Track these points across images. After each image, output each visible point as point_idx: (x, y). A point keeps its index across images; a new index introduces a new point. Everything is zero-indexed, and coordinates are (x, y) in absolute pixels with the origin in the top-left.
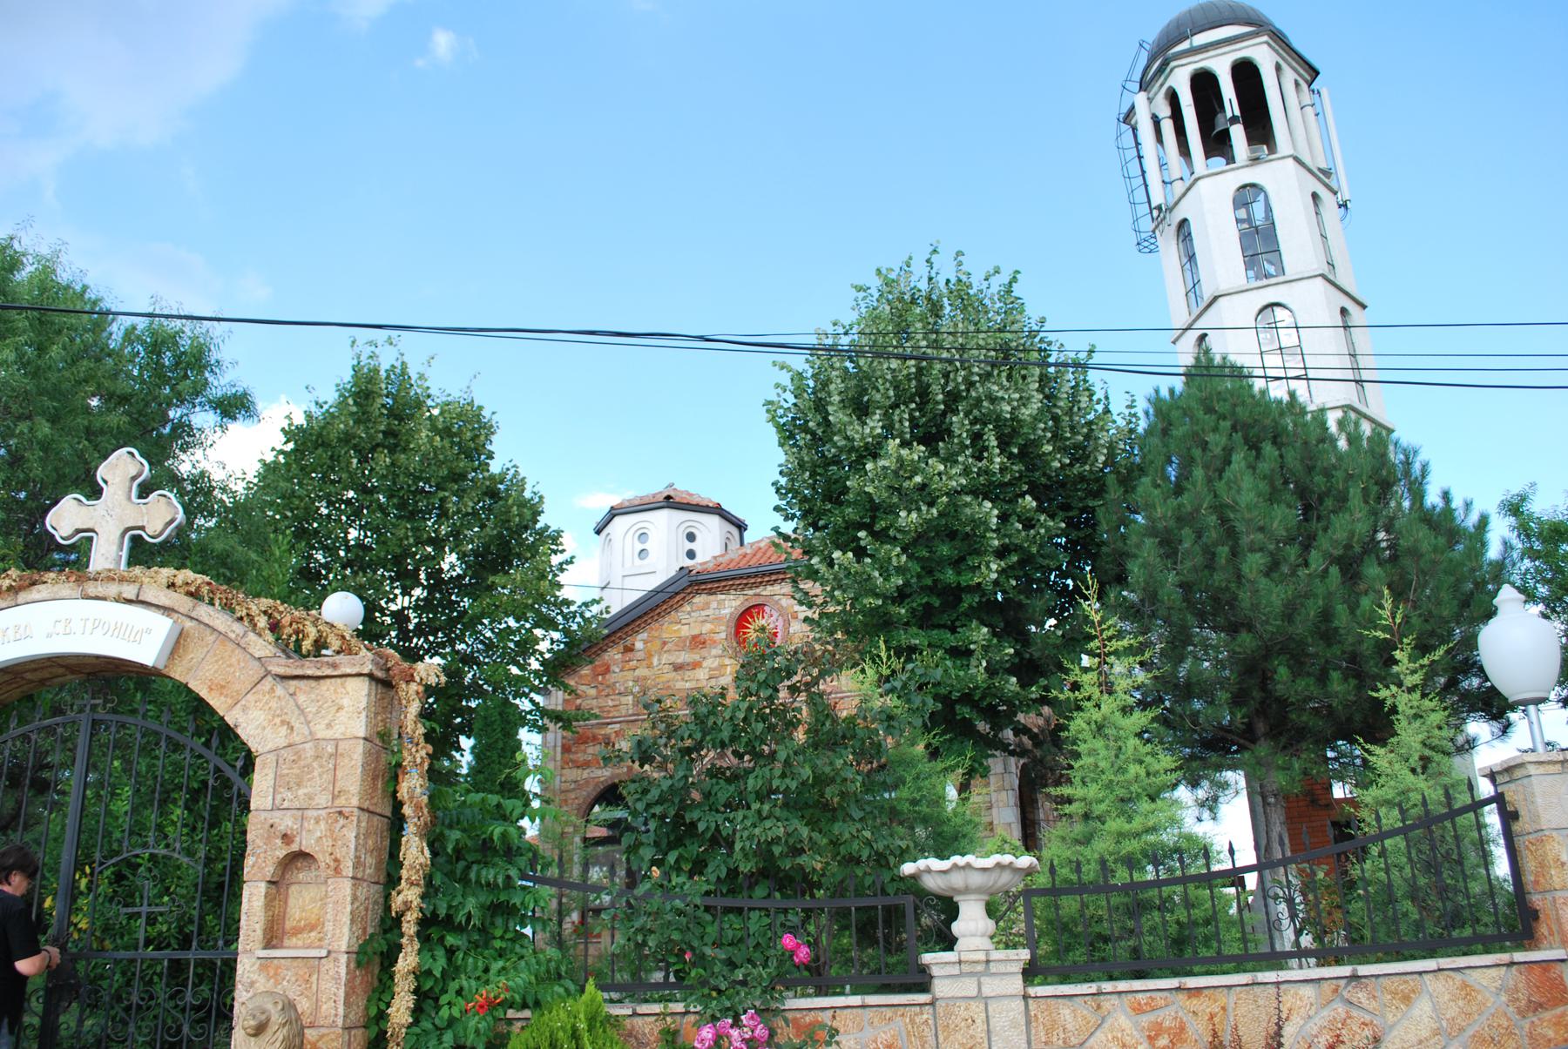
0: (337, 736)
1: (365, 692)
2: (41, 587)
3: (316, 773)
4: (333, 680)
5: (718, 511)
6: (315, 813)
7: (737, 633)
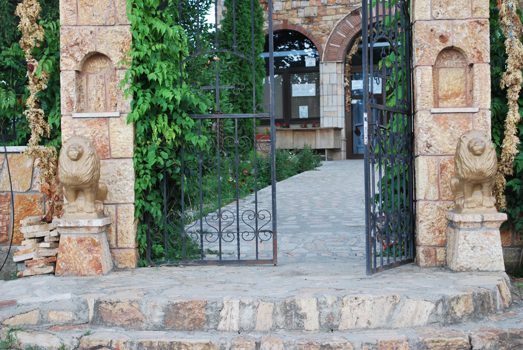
6: (461, 22)
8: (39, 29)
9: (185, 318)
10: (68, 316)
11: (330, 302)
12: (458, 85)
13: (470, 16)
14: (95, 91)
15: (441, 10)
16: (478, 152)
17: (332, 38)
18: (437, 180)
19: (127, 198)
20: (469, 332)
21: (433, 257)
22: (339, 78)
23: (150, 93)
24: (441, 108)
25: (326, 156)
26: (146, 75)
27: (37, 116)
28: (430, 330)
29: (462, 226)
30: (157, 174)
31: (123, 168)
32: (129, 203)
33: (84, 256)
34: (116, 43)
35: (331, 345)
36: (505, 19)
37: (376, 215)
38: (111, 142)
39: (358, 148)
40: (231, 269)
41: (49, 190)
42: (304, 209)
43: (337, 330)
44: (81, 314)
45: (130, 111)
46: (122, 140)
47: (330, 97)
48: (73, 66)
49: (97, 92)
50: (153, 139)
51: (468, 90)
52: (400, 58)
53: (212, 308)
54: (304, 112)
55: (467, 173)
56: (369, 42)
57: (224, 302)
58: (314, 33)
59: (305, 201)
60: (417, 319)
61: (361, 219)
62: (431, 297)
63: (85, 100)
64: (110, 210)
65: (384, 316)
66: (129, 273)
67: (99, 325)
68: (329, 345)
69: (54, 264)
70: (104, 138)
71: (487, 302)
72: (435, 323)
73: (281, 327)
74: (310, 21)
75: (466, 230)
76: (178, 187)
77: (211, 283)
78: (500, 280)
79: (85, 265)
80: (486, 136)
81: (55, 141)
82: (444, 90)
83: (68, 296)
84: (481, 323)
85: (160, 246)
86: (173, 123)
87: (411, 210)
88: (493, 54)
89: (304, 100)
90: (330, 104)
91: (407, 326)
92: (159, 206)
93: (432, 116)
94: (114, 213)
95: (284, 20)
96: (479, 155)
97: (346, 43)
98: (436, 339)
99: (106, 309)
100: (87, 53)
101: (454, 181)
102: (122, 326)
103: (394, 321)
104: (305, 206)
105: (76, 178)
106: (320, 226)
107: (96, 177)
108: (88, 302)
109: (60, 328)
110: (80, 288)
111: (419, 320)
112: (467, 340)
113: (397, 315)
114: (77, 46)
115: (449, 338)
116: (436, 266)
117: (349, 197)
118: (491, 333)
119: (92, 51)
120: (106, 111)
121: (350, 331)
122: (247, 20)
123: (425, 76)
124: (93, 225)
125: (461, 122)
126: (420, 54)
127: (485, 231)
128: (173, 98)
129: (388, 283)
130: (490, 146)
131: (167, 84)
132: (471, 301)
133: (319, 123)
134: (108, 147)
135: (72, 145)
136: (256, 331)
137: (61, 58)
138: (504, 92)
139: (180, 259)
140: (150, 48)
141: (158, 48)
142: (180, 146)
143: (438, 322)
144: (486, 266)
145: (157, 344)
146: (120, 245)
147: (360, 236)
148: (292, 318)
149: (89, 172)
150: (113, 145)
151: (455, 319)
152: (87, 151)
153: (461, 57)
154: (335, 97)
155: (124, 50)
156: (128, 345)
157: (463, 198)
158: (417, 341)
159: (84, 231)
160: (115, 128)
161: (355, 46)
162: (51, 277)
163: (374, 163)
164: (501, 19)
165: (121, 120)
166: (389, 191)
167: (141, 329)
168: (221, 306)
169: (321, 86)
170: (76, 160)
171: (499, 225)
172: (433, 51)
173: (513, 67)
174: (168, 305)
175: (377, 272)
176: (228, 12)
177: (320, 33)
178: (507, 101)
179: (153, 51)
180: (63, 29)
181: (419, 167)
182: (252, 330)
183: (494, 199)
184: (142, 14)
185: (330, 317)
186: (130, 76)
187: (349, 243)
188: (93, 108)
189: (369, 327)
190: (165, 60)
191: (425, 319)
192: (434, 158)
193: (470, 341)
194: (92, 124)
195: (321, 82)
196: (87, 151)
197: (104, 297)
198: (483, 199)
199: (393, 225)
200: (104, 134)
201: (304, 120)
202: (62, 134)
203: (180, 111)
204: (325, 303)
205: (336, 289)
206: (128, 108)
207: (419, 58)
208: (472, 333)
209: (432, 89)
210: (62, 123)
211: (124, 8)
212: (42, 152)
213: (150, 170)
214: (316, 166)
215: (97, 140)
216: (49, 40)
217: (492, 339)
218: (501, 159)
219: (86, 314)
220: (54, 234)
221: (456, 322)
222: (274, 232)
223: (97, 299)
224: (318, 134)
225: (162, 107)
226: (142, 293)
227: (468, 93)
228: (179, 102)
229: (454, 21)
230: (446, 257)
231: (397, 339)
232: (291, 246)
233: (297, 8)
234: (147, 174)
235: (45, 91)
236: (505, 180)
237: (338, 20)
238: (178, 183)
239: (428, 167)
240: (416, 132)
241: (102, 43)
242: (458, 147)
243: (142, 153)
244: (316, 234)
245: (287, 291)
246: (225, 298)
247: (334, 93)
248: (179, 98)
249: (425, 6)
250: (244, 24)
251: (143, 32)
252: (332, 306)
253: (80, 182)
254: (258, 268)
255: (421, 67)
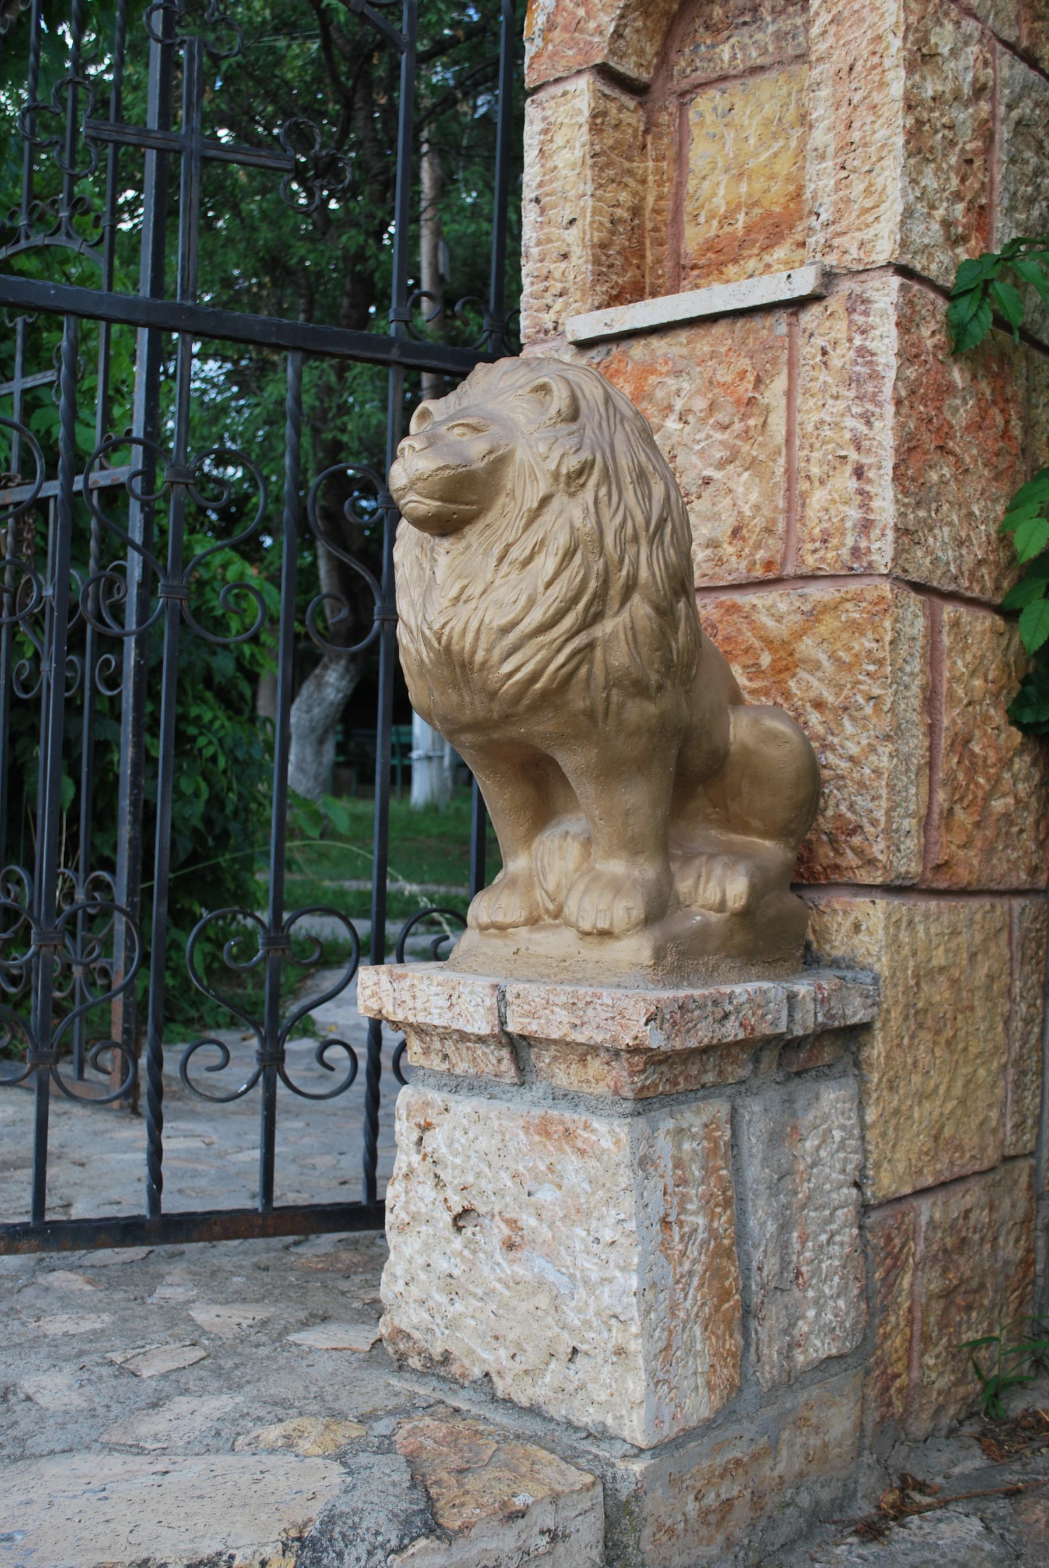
7: (903, 223)
125: (724, 376)
207: (538, 42)
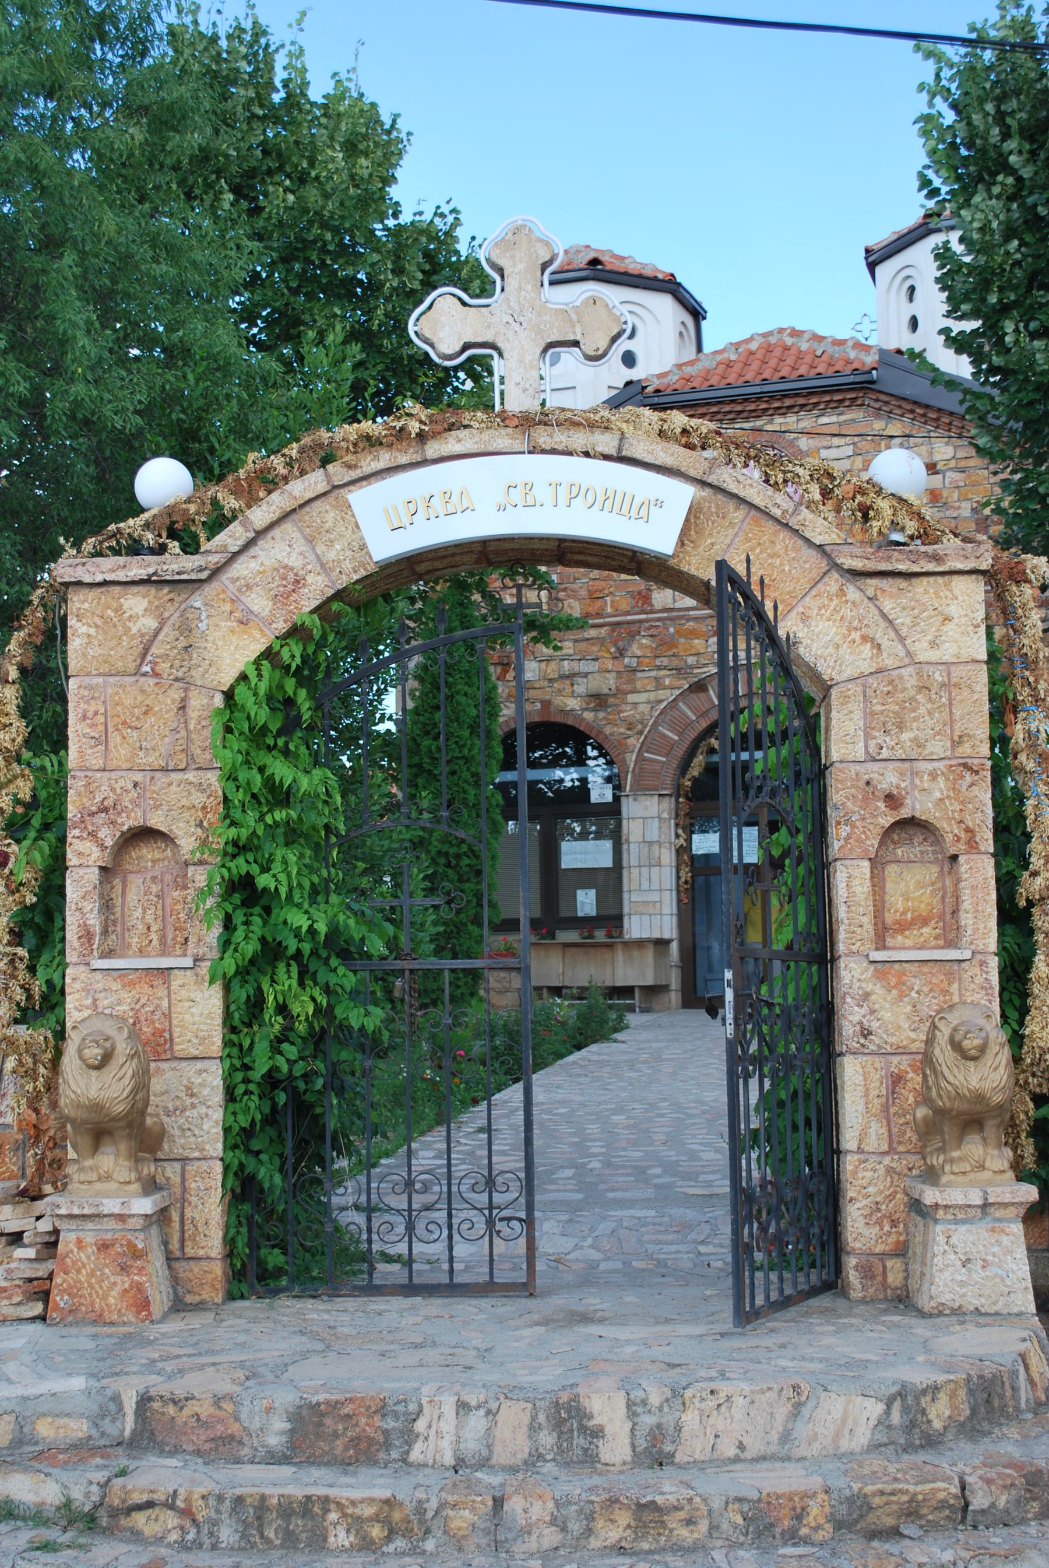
0: (947, 658)
1: (981, 597)
2: (462, 433)
3: (922, 710)
4: (932, 579)
5: (670, 286)
6: (930, 766)
8: (23, 776)
9: (336, 1435)
10: (79, 1428)
11: (655, 1400)
12: (926, 899)
13: (949, 753)
14: (140, 910)
15: (888, 739)
16: (973, 1052)
17: (648, 740)
18: (886, 1108)
19: (207, 1147)
20: (961, 1465)
21: (879, 1278)
22: (665, 829)
23: (260, 915)
24: (890, 948)
25: (637, 1001)
26: (253, 878)
27: (12, 962)
28: (875, 1463)
29: (941, 1212)
30: (273, 1090)
31: (200, 1080)
32: (212, 1158)
33: (112, 1280)
34: (189, 809)
35: (659, 1502)
36: (1022, 757)
37: (754, 1192)
38: (175, 1022)
39: (706, 981)
40: (435, 1306)
41: (35, 1126)
42: (593, 1150)
43: (672, 1463)
44: (106, 1424)
45: (215, 954)
46: (197, 1019)
47: (645, 870)
48: (94, 856)
49: (144, 913)
50: (267, 1017)
51: (948, 911)
52: (801, 838)
53: (396, 1415)
54: (586, 902)
55: (949, 1098)
56: (733, 750)
57: (424, 1401)
58: (608, 730)
59: (593, 1128)
60: (847, 1437)
61: (718, 1176)
62: (876, 1387)
63: (119, 929)
64: (169, 1172)
65: (774, 1432)
66: (208, 1317)
67: (146, 1449)
68: (654, 1502)
69: (45, 1296)
70: (158, 1013)
71: (999, 1395)
72: (885, 1445)
73: (548, 1457)
74: (599, 705)
75: (949, 1222)
76: (316, 1118)
77: (392, 1347)
78: (1024, 1340)
79: (112, 1301)
80: (989, 1016)
81: (52, 1018)
82: (896, 911)
83: (78, 1383)
84: (986, 1445)
85: (277, 1251)
86: (309, 982)
87: (829, 1172)
88: (1001, 829)
89: (587, 877)
90: (645, 885)
91: (824, 1453)
92: (277, 1161)
93: (872, 967)
94: (178, 1180)
95: (542, 702)
96: (974, 1059)
97: (680, 752)
98: (889, 1488)
99: (163, 1414)
100: (125, 828)
101: (922, 1112)
102: (198, 1453)
103: (797, 1443)
104: (594, 1140)
105: (96, 1107)
106: (627, 1195)
107: (140, 1105)
108: (123, 1397)
109: (61, 1457)
110: (104, 1359)
111: (851, 1440)
112: (955, 1490)
113: (802, 1430)
114: (103, 815)
115: (916, 1484)
116: (886, 1299)
117: (691, 1116)
118: (1008, 1471)
119: (136, 824)
120: (164, 953)
121: (700, 1465)
122: (464, 711)
123: (856, 882)
124: (133, 1212)
125: (934, 980)
126: (844, 834)
127: (990, 1226)
128: (311, 927)
129: (783, 1346)
130: (998, 1036)
131: (297, 898)
132: (962, 1393)
133: (622, 926)
134: (167, 1035)
135: (90, 1034)
136: (492, 1467)
137: (69, 840)
138: (1026, 914)
139: (321, 1279)
140: (261, 818)
141: (278, 818)
142: (322, 1028)
143: (892, 1443)
144: (995, 1303)
145: (275, 1501)
146: (189, 1251)
147: (716, 1219)
148: (572, 1437)
149: (125, 1095)
150: (178, 1029)
151: (929, 1435)
152: (123, 1048)
153: (931, 839)
154: (655, 870)
155: (205, 824)
156: (212, 1502)
157: (942, 1150)
158: (847, 1493)
159: (112, 1224)
160: (184, 993)
161: (700, 759)
162: (38, 1327)
163: (747, 1076)
164: (1015, 758)
165: (197, 975)
166: (781, 1124)
167: (238, 1461)
168: (417, 1409)
169: (625, 847)
170: (97, 1068)
171: (1022, 1211)
172: (871, 827)
173: (1042, 861)
174: (300, 1407)
175: (757, 1318)
176: (422, 693)
177: (622, 730)
178: (1031, 932)
179: (267, 825)
180: (74, 777)
181: (846, 1078)
182: (484, 1463)
183: (1009, 1153)
184: (244, 745)
185: (657, 1434)
186: (219, 880)
187: (692, 1236)
188: (135, 947)
189: (742, 1456)
190: (293, 842)
191: (863, 1437)
192: (877, 1059)
193: (963, 1488)
194: (132, 984)
195: (624, 838)
196: (123, 1048)
197: (155, 1383)
198: (986, 1153)
199: (791, 1207)
200: (158, 1006)
201: (587, 919)
202: (67, 1006)
203: (324, 953)
204: (644, 1402)
205: (668, 1365)
206: (211, 948)
207: (842, 842)
208: (968, 1470)
209: (871, 908)
210: (68, 980)
211: (207, 733)
212: (21, 1041)
213: (259, 1084)
214: (616, 1030)
215: (142, 1019)
216: (43, 795)
217: (1012, 1485)
218: (1022, 1059)
219: (118, 1424)
220: (44, 1226)
221: (931, 1441)
222: (529, 1222)
223: (141, 1389)
224: (620, 955)
225: (286, 947)
226: (240, 1374)
227: (948, 917)
228: (323, 938)
229: (915, 764)
230: (906, 1278)
231: (802, 1488)
232: (565, 1244)
233: (571, 676)
234: (252, 1093)
235: (33, 906)
236: (1031, 1105)
237: (661, 701)
238: (318, 1110)
239: (865, 1079)
240: (837, 1001)
241: (157, 807)
242: (930, 1041)
243: (241, 1046)
244: (620, 1213)
245: (560, 1371)
246: (426, 1390)
247: (653, 862)
248: (322, 927)
249: (852, 732)
250: (457, 720)
251: (248, 784)
252: (660, 1409)
253: (106, 1115)
254: (493, 1301)
255: (848, 862)
